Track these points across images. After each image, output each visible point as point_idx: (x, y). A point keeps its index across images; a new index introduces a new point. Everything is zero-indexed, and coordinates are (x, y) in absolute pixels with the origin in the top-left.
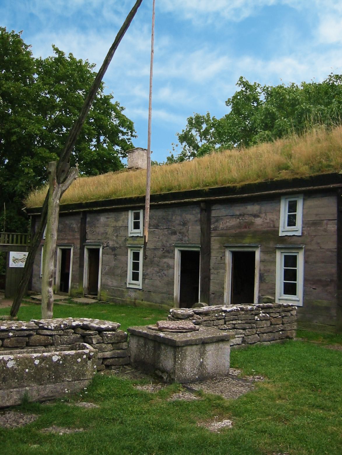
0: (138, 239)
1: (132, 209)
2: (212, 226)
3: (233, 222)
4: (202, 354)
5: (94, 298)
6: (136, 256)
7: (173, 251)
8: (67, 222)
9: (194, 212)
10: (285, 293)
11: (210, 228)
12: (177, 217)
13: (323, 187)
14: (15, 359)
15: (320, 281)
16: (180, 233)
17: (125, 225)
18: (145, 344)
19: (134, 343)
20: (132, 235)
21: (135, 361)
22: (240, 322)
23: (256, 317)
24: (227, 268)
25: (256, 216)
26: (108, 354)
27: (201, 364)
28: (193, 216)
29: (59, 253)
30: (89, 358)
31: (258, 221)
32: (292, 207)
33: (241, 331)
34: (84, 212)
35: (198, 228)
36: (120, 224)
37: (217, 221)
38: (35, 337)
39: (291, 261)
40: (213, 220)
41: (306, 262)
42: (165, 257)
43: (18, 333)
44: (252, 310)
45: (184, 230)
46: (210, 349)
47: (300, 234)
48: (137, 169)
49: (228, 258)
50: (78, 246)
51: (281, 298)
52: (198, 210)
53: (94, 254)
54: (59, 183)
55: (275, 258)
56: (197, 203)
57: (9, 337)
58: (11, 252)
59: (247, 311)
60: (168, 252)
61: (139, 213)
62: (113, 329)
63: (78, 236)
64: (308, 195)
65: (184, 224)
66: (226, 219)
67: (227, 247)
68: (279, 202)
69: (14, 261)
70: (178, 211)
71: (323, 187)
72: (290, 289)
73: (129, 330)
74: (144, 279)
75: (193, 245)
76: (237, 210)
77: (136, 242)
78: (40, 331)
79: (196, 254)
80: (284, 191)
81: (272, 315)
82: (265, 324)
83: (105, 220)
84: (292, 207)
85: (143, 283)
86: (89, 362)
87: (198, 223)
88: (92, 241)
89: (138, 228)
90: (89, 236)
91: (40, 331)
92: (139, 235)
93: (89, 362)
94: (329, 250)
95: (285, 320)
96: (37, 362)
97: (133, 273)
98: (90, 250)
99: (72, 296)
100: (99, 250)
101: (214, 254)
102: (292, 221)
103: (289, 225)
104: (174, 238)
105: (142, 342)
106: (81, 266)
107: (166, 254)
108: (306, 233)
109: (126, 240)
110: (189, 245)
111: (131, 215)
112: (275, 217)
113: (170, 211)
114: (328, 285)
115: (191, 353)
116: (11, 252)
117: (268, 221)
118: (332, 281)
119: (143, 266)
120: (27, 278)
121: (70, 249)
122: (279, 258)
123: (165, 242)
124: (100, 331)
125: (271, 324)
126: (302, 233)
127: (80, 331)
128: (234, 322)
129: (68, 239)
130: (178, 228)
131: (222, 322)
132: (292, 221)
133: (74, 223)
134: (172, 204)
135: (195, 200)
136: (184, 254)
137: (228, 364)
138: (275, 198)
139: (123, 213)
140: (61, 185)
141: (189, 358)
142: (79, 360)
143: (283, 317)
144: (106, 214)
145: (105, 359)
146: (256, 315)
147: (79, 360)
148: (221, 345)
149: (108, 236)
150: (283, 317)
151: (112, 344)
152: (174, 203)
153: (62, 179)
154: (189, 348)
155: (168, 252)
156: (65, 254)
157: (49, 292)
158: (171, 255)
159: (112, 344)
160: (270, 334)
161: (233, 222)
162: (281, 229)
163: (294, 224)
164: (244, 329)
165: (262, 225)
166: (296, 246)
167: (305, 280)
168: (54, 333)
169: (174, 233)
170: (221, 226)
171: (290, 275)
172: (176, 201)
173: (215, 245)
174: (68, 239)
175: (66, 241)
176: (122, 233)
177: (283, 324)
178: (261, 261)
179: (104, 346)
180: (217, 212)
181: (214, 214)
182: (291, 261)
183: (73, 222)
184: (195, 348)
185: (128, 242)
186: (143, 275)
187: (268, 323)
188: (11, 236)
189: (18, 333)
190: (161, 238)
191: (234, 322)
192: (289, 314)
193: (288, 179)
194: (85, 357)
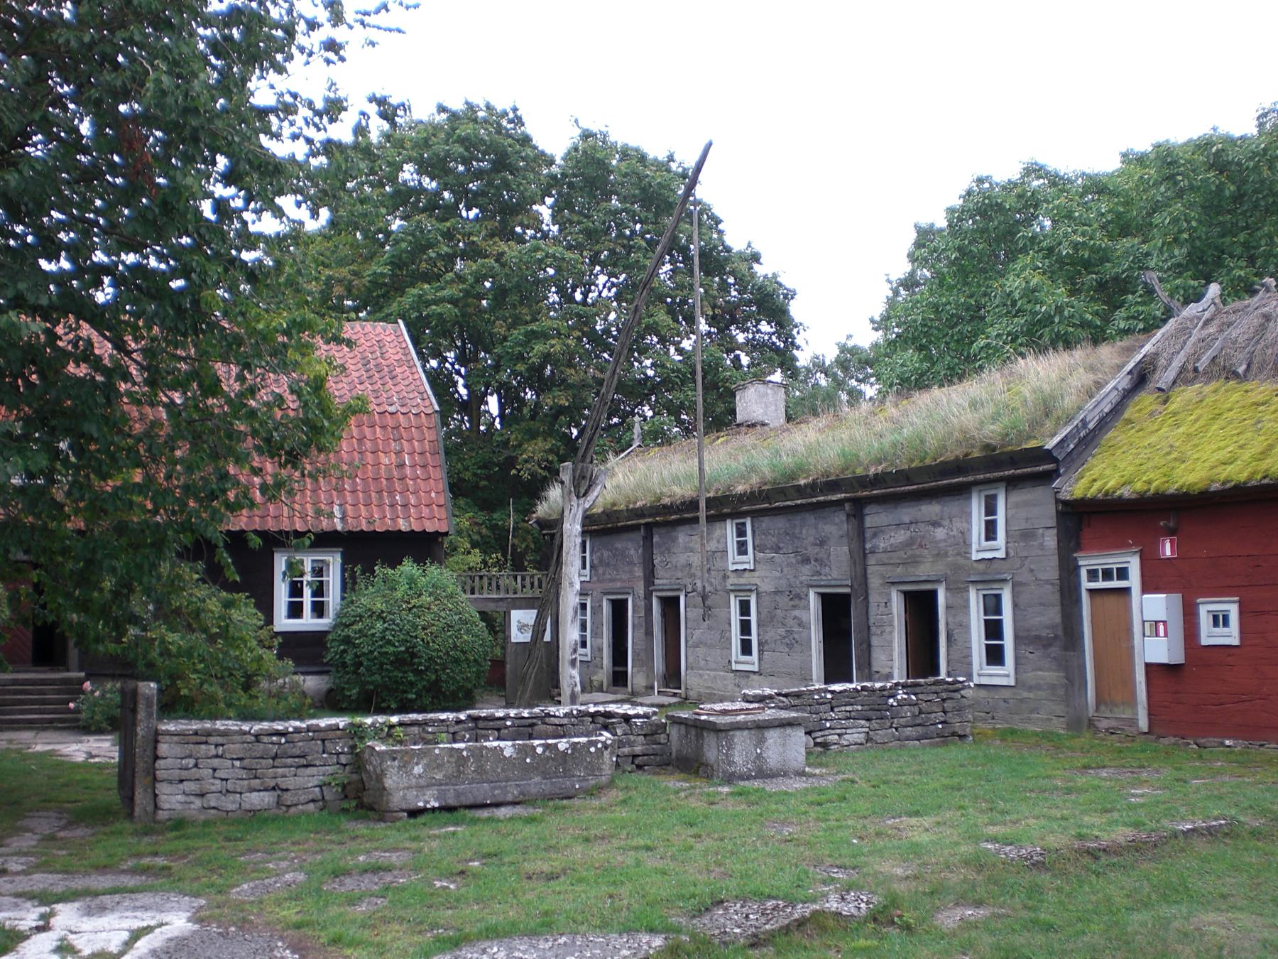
0: (747, 574)
1: (732, 516)
2: (868, 546)
3: (901, 536)
4: (761, 742)
5: (675, 695)
6: (745, 608)
7: (807, 595)
8: (619, 545)
9: (837, 520)
10: (988, 664)
11: (864, 549)
12: (809, 529)
13: (1029, 470)
14: (513, 746)
15: (1038, 638)
16: (816, 560)
17: (721, 547)
18: (687, 733)
19: (674, 732)
20: (735, 567)
21: (677, 759)
22: (859, 708)
23: (891, 701)
24: (896, 623)
25: (936, 524)
26: (638, 749)
27: (759, 756)
28: (835, 527)
29: (606, 608)
30: (606, 747)
31: (940, 533)
32: (990, 509)
33: (863, 722)
34: (646, 524)
35: (846, 549)
36: (712, 546)
37: (875, 535)
38: (541, 727)
39: (993, 605)
40: (868, 535)
41: (1015, 606)
42: (794, 607)
43: (517, 722)
44: (882, 689)
45: (822, 555)
46: (773, 736)
47: (1004, 556)
48: (754, 425)
49: (897, 604)
50: (641, 593)
51: (983, 673)
52: (842, 517)
53: (670, 604)
54: (578, 497)
55: (967, 601)
56: (839, 503)
57: (507, 727)
58: (513, 612)
59: (873, 690)
60: (798, 597)
61: (744, 524)
62: (646, 716)
63: (639, 572)
64: (1012, 483)
65: (822, 543)
66: (890, 529)
67: (812, 586)
68: (970, 498)
69: (520, 630)
70: (810, 518)
71: (1029, 470)
72: (995, 655)
73: (667, 717)
74: (761, 651)
75: (839, 583)
76: (907, 513)
77: (742, 581)
78: (547, 720)
79: (846, 597)
80: (970, 478)
81: (920, 696)
82: (907, 712)
83: (687, 539)
84: (990, 509)
85: (760, 659)
86: (607, 754)
87: (845, 540)
88: (664, 581)
89: (746, 553)
90: (659, 572)
91: (547, 720)
92: (747, 566)
93: (607, 754)
94: (1047, 582)
95: (948, 705)
96: (539, 750)
97: (742, 640)
98: (662, 599)
99: (633, 694)
100: (678, 598)
101: (874, 598)
102: (990, 532)
103: (988, 539)
104: (806, 569)
105: (683, 727)
106: (649, 633)
107: (796, 602)
108: (1012, 553)
109: (725, 577)
110: (833, 583)
111: (730, 528)
112: (965, 525)
113: (797, 520)
114: (1050, 645)
115: (742, 741)
116: (513, 612)
117: (955, 533)
118: (1056, 637)
119: (759, 625)
120: (545, 655)
121: (627, 600)
122: (975, 600)
123: (792, 580)
124: (627, 718)
125: (920, 712)
126: (1007, 553)
127: (601, 720)
128: (848, 708)
129: (621, 580)
130: (812, 551)
131: (827, 707)
132: (990, 532)
133: (631, 547)
134: (797, 505)
135: (834, 498)
136: (826, 599)
137: (802, 758)
138: (962, 491)
139: (718, 525)
140: (581, 501)
141: (739, 747)
142: (592, 750)
143: (943, 700)
144: (687, 527)
145: (635, 756)
146: (890, 697)
147: (592, 750)
148: (789, 730)
149: (693, 571)
150: (943, 700)
151: (645, 735)
152: (802, 505)
153: (583, 491)
154: (738, 733)
155: (798, 598)
156: (619, 609)
157: (572, 677)
158: (803, 603)
159: (645, 735)
160: (919, 728)
161: (901, 536)
162: (974, 547)
163: (995, 539)
164: (868, 720)
165: (945, 541)
166: (998, 577)
167: (1017, 638)
168: (565, 721)
169: (806, 560)
170: (882, 545)
171: (993, 630)
172: (803, 501)
173: (874, 582)
174: (621, 580)
175: (619, 585)
176: (719, 564)
177: (945, 712)
178: (948, 607)
179: (632, 738)
180: (875, 518)
181: (869, 521)
182: (993, 605)
183: (630, 544)
184: (746, 733)
185: (730, 581)
186: (760, 644)
187: (916, 710)
188: (519, 578)
189: (517, 722)
190: (785, 570)
191: (848, 708)
192: (957, 695)
193: (957, 458)
194: (600, 745)
